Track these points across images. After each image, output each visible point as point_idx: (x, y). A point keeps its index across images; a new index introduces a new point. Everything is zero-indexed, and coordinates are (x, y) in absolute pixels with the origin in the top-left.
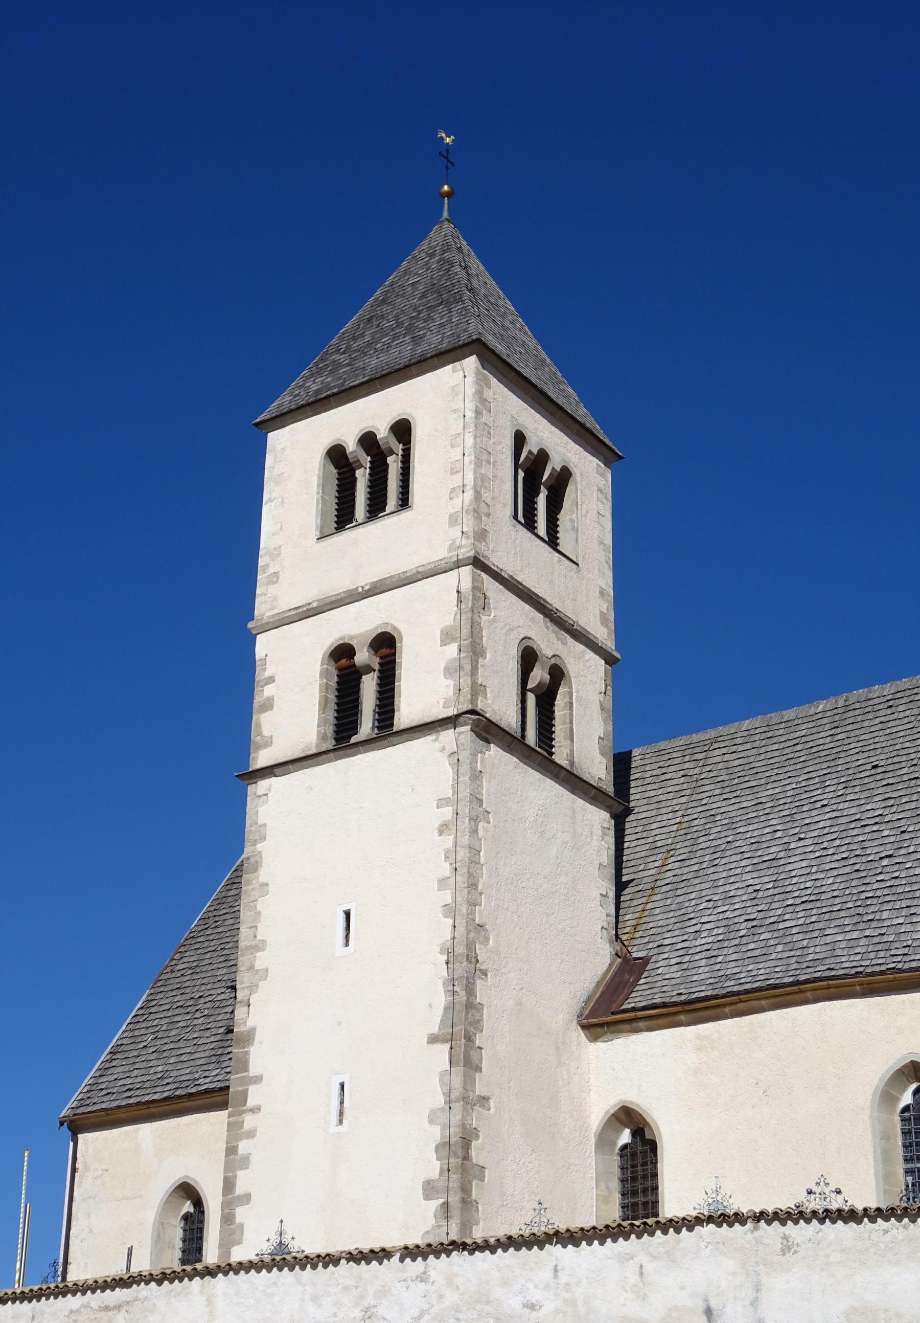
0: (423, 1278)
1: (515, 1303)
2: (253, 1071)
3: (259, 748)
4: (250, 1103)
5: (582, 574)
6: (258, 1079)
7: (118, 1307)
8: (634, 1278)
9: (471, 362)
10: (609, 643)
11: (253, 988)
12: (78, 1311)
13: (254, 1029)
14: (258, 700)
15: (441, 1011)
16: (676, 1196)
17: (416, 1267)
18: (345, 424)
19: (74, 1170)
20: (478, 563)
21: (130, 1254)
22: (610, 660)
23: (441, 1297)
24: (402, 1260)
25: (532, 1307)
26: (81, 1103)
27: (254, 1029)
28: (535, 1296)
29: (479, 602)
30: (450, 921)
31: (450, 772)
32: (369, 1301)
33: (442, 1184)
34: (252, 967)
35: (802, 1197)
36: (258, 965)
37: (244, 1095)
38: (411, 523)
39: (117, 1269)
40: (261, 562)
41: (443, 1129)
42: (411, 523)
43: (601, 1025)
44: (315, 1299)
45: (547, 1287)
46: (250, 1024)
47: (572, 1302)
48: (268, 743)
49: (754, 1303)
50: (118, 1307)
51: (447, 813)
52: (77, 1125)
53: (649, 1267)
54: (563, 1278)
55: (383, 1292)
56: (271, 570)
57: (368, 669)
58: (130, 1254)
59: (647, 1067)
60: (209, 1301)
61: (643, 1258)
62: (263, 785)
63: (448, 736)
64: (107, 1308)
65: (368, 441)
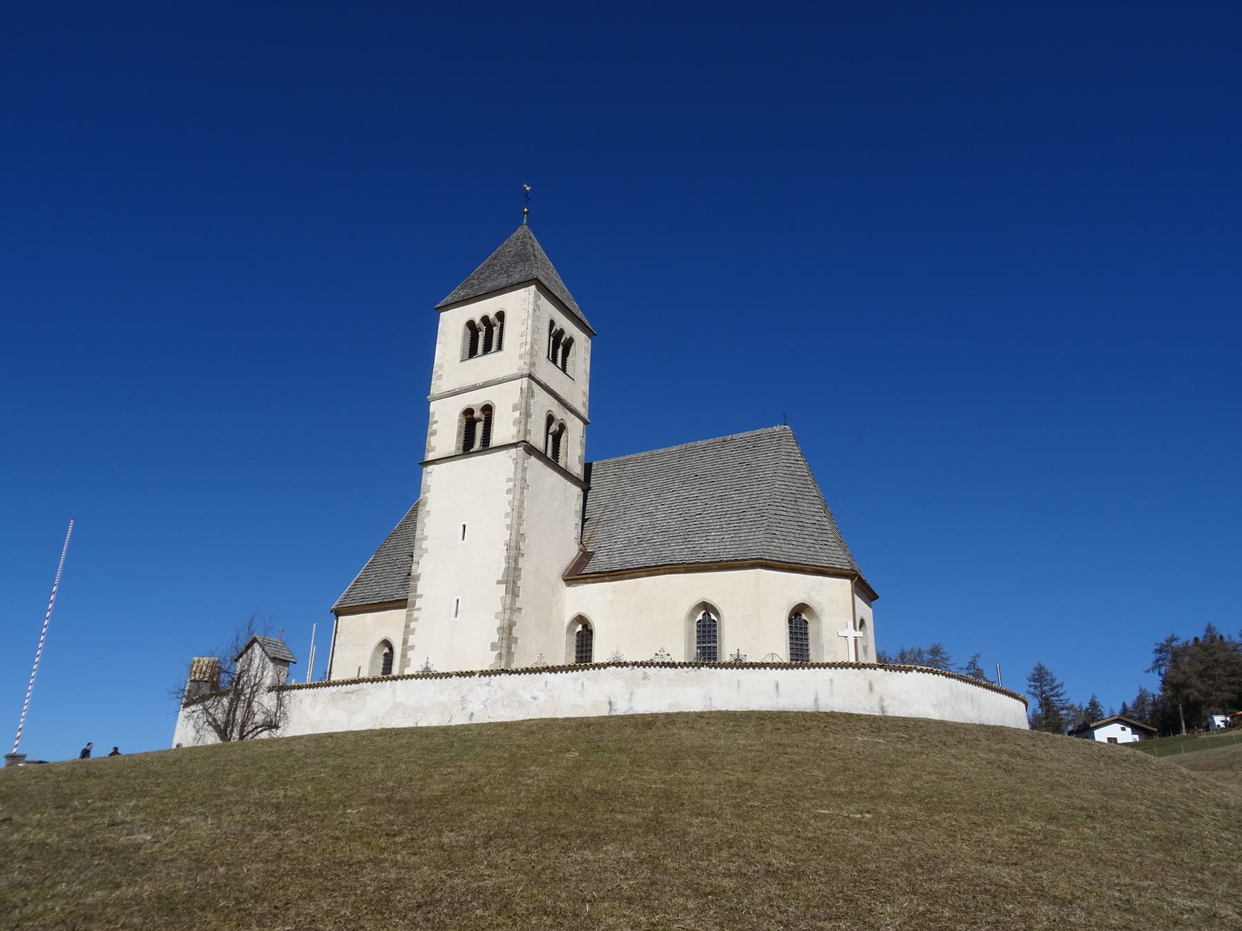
0: (488, 684)
2: (419, 592)
5: (576, 384)
6: (421, 596)
8: (579, 688)
9: (533, 288)
10: (586, 416)
11: (421, 556)
16: (600, 653)
20: (530, 376)
22: (585, 422)
26: (341, 603)
28: (536, 694)
29: (530, 394)
35: (653, 656)
37: (414, 603)
38: (501, 356)
39: (353, 676)
42: (501, 356)
48: (433, 449)
52: (338, 613)
55: (471, 690)
57: (480, 420)
59: (590, 599)
61: (584, 679)
62: (430, 468)
63: (513, 451)
65: (485, 319)
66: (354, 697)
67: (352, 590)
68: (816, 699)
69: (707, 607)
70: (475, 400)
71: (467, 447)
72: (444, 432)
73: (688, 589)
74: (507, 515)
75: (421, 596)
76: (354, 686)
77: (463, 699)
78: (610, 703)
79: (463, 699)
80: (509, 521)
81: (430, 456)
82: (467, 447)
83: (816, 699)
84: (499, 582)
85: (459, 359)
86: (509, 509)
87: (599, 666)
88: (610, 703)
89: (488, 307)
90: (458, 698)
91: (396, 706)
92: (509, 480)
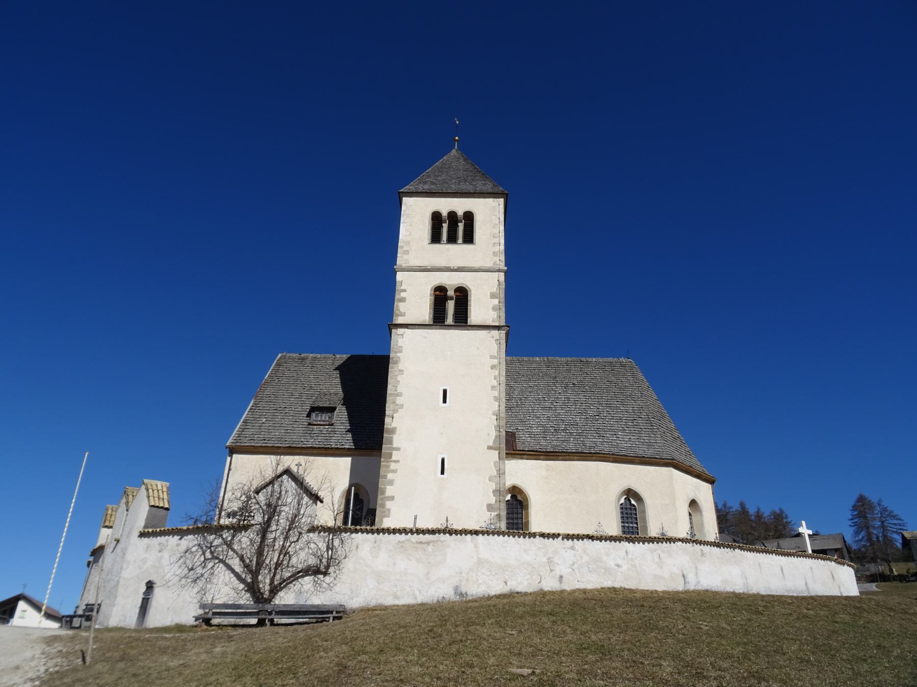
0: (572, 548)
1: (612, 564)
2: (395, 445)
3: (398, 315)
4: (394, 458)
6: (398, 449)
7: (428, 543)
8: (657, 559)
11: (395, 411)
12: (403, 542)
13: (395, 428)
14: (397, 297)
15: (494, 438)
16: (537, 521)
17: (569, 543)
18: (445, 205)
19: (230, 469)
21: (415, 518)
23: (581, 557)
24: (563, 539)
25: (618, 566)
26: (236, 441)
27: (395, 428)
28: (620, 562)
30: (497, 403)
31: (496, 347)
32: (550, 555)
33: (497, 506)
34: (394, 403)
35: (484, 525)
36: (398, 402)
37: (390, 455)
38: (449, 250)
39: (409, 525)
40: (400, 244)
41: (496, 484)
42: (449, 250)
43: (512, 454)
44: (525, 551)
45: (624, 559)
46: (394, 425)
47: (635, 566)
48: (403, 315)
49: (697, 574)
50: (428, 543)
51: (495, 362)
52: (233, 451)
53: (662, 556)
54: (630, 556)
55: (556, 552)
56: (405, 249)
57: (451, 298)
58: (415, 518)
59: (525, 473)
60: (476, 546)
61: (659, 552)
62: (400, 331)
63: (495, 333)
64: (421, 543)
66: (430, 548)
67: (242, 430)
68: (806, 584)
69: (630, 493)
70: (451, 281)
71: (438, 319)
72: (413, 298)
73: (618, 477)
74: (493, 388)
75: (398, 449)
76: (428, 537)
77: (550, 561)
78: (684, 576)
79: (550, 561)
80: (496, 394)
81: (400, 320)
82: (438, 319)
83: (806, 584)
84: (489, 448)
85: (429, 241)
86: (495, 383)
87: (533, 535)
88: (684, 576)
89: (460, 205)
90: (545, 560)
91: (480, 562)
92: (492, 357)
